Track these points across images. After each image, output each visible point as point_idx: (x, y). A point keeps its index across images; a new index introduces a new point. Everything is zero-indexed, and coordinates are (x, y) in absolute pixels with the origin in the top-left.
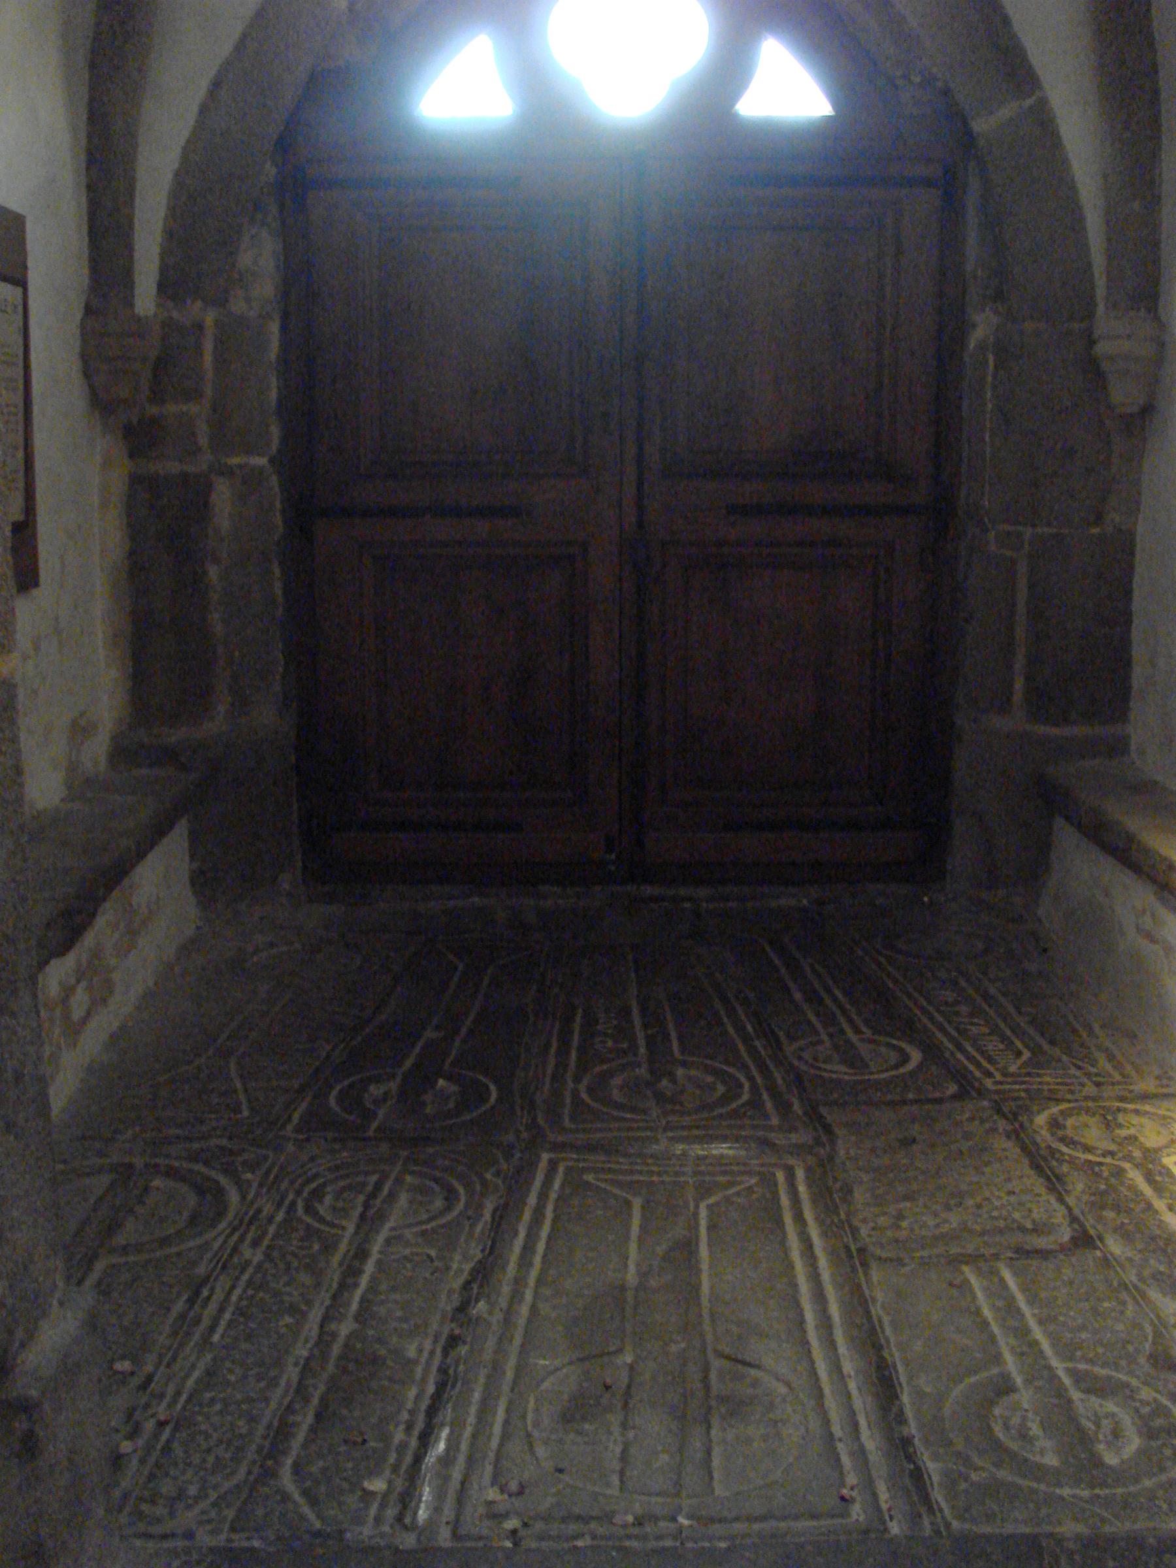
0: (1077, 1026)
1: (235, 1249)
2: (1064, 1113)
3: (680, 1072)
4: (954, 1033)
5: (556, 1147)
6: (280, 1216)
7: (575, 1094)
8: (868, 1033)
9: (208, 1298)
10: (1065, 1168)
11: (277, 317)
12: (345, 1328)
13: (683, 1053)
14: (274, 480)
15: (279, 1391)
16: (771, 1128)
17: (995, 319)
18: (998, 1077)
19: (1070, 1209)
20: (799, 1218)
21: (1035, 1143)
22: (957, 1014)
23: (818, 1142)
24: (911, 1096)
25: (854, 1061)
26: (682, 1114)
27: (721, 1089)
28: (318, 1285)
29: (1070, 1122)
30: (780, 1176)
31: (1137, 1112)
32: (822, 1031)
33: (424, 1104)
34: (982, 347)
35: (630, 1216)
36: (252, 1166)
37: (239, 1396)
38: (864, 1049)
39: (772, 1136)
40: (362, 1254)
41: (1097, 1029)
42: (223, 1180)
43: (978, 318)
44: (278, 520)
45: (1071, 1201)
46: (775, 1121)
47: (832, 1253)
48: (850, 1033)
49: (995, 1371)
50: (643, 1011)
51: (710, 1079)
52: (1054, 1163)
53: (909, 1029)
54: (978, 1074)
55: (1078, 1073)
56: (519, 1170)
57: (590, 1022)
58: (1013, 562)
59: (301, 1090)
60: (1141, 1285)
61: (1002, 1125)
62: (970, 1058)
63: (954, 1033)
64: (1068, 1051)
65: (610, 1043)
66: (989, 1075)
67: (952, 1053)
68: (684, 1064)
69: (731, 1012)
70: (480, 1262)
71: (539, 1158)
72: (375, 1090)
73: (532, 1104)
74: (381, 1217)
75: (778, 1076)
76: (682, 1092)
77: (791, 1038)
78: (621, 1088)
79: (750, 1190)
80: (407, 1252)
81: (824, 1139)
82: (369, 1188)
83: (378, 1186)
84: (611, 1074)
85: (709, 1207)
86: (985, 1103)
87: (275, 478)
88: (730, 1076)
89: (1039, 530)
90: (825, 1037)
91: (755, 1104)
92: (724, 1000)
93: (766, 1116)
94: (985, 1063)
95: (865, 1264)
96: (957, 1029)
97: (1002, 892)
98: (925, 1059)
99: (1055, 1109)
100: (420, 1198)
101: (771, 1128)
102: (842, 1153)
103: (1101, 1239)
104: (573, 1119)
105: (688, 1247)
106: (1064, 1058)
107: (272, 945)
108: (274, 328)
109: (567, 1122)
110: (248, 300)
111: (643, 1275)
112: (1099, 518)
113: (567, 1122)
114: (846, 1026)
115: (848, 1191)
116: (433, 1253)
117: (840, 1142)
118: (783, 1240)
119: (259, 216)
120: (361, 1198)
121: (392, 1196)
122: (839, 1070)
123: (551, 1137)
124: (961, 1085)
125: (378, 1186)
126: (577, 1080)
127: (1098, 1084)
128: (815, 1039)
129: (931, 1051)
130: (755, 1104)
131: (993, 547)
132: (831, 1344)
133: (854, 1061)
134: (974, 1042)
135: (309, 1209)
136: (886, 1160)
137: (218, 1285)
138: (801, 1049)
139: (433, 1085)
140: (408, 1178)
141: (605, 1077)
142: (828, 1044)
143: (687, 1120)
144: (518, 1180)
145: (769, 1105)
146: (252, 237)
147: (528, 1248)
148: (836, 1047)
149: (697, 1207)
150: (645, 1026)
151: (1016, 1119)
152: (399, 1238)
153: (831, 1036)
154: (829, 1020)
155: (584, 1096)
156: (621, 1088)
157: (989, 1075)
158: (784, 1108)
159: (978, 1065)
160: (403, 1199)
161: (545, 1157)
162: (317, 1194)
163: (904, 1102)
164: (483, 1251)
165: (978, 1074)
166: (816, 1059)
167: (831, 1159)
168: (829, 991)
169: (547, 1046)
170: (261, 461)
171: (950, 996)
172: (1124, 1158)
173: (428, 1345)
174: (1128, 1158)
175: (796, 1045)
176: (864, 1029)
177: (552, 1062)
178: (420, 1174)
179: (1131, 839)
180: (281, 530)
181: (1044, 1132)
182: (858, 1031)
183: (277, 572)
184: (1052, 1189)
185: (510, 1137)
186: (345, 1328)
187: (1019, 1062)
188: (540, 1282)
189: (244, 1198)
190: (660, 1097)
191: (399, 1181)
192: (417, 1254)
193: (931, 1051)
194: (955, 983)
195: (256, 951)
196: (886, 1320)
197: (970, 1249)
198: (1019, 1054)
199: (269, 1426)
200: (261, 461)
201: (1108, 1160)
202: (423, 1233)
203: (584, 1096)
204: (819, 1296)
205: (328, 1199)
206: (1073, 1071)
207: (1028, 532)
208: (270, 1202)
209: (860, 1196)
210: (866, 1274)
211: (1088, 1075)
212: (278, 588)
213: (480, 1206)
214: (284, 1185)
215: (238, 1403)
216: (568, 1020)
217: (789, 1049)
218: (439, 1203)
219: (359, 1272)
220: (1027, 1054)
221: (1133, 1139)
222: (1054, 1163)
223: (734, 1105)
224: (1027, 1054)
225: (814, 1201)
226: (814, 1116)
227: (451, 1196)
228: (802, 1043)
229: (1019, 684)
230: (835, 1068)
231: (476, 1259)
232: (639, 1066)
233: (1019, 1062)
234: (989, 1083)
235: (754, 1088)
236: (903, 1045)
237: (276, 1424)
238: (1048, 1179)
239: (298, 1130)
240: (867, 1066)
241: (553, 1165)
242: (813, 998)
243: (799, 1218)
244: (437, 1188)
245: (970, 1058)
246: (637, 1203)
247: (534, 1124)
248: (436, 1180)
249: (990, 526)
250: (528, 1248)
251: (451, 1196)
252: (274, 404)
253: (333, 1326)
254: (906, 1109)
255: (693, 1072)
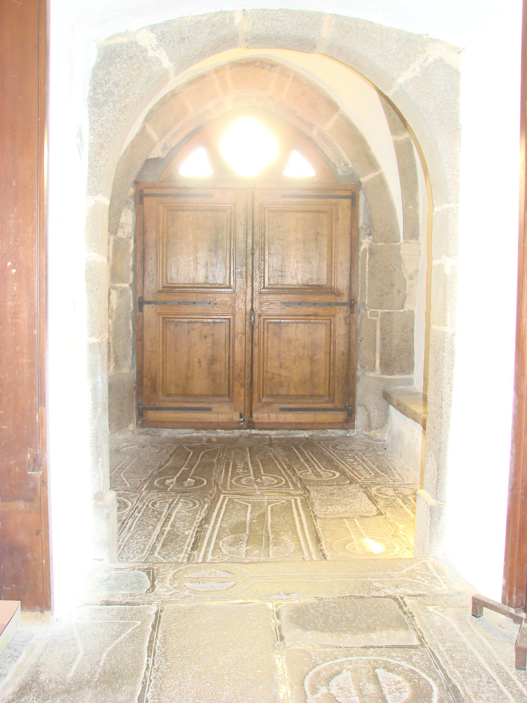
0: (391, 468)
1: (132, 514)
2: (381, 488)
3: (263, 477)
4: (351, 469)
5: (224, 494)
6: (145, 507)
7: (231, 482)
8: (324, 469)
9: (127, 523)
10: (378, 499)
11: (133, 238)
13: (264, 473)
14: (131, 292)
15: (151, 540)
16: (291, 490)
17: (369, 241)
18: (363, 479)
19: (377, 508)
20: (297, 509)
21: (371, 494)
22: (353, 465)
23: (305, 493)
24: (335, 484)
25: (317, 474)
26: (264, 487)
27: (276, 481)
28: (158, 521)
29: (383, 489)
30: (293, 501)
31: (404, 487)
32: (309, 468)
34: (365, 250)
36: (133, 497)
37: (140, 541)
38: (322, 473)
39: (291, 492)
40: (170, 515)
41: (397, 469)
42: (126, 500)
43: (363, 241)
44: (132, 305)
45: (378, 506)
46: (292, 488)
47: (307, 516)
48: (318, 469)
49: (349, 538)
50: (252, 463)
51: (273, 479)
52: (376, 498)
53: (337, 468)
54: (357, 478)
55: (389, 479)
56: (214, 498)
57: (235, 466)
58: (375, 321)
59: (145, 481)
60: (394, 522)
61: (362, 490)
62: (355, 475)
63: (351, 469)
64: (386, 473)
65: (241, 471)
66: (360, 478)
67: (350, 474)
68: (264, 476)
69: (280, 464)
71: (220, 496)
72: (168, 481)
73: (218, 485)
74: (174, 508)
75: (294, 478)
76: (264, 482)
77: (299, 470)
78: (245, 481)
79: (283, 503)
81: (307, 493)
82: (170, 502)
84: (242, 478)
85: (271, 507)
86: (358, 485)
87: (131, 291)
88: (279, 478)
89: (383, 311)
90: (309, 469)
91: (287, 484)
92: (278, 461)
93: (289, 487)
94: (359, 476)
95: (315, 519)
96: (352, 468)
97: (373, 432)
98: (340, 475)
99: (379, 487)
101: (291, 490)
102: (312, 496)
103: (385, 514)
104: (230, 488)
105: (264, 515)
106: (385, 475)
107: (128, 446)
108: (132, 241)
109: (228, 488)
110: (124, 233)
111: (252, 520)
112: (402, 307)
113: (228, 488)
114: (316, 467)
115: (313, 504)
117: (311, 493)
118: (292, 514)
119: (128, 205)
120: (168, 504)
121: (177, 504)
122: (313, 477)
123: (223, 491)
124: (350, 481)
126: (231, 479)
127: (394, 481)
128: (306, 470)
129: (343, 473)
130: (287, 484)
131: (369, 316)
132: (304, 533)
133: (317, 474)
134: (357, 471)
135: (153, 505)
136: (325, 498)
137: (130, 521)
138: (302, 473)
139: (187, 480)
141: (240, 479)
142: (311, 471)
143: (265, 488)
144: (214, 502)
145: (291, 485)
146: (126, 212)
147: (218, 516)
148: (313, 472)
149: (267, 506)
150: (253, 467)
151: (366, 488)
152: (181, 512)
153: (312, 470)
154: (311, 466)
155: (234, 483)
156: (245, 481)
157: (360, 478)
158: (295, 485)
159: (357, 476)
160: (180, 504)
161: (222, 496)
162: (155, 503)
163: (332, 485)
165: (357, 478)
166: (306, 475)
167: (308, 497)
168: (312, 459)
169: (222, 471)
170: (127, 285)
171: (352, 460)
172: (397, 497)
173: (191, 532)
174: (399, 497)
175: (301, 472)
176: (322, 468)
177: (223, 475)
178: (185, 499)
179: (406, 407)
180: (132, 308)
181: (374, 492)
182: (320, 468)
183: (131, 322)
184: (374, 503)
185: (211, 492)
186: (168, 529)
187: (370, 476)
188: (222, 520)
189: (132, 504)
190: (257, 483)
191: (179, 500)
193: (343, 473)
194: (354, 457)
195: (123, 448)
196: (320, 529)
197: (347, 516)
198: (371, 474)
199: (150, 546)
200: (127, 285)
201: (392, 497)
202: (187, 511)
203: (234, 483)
204: (301, 524)
205: (158, 504)
206: (387, 478)
207: (380, 311)
209: (316, 505)
210: (315, 521)
211: (391, 479)
212: (131, 327)
214: (145, 501)
215: (141, 542)
216: (228, 465)
217: (298, 473)
218: (191, 505)
219: (170, 518)
220: (373, 474)
221: (401, 493)
222: (376, 498)
223: (280, 485)
224: (373, 474)
225: (302, 506)
226: (304, 488)
227: (195, 504)
228: (302, 471)
229: (378, 361)
230: (312, 477)
232: (251, 476)
233: (370, 476)
234: (360, 481)
235: (286, 481)
236: (334, 472)
237: (152, 546)
238: (373, 501)
239: (146, 489)
240: (322, 477)
241: (224, 498)
242: (307, 460)
243: (297, 509)
244: (190, 502)
245: (355, 475)
246: (250, 505)
247: (218, 488)
249: (368, 309)
250: (218, 516)
251: (195, 504)
252: (131, 266)
253: (164, 528)
254: (333, 487)
255: (267, 477)
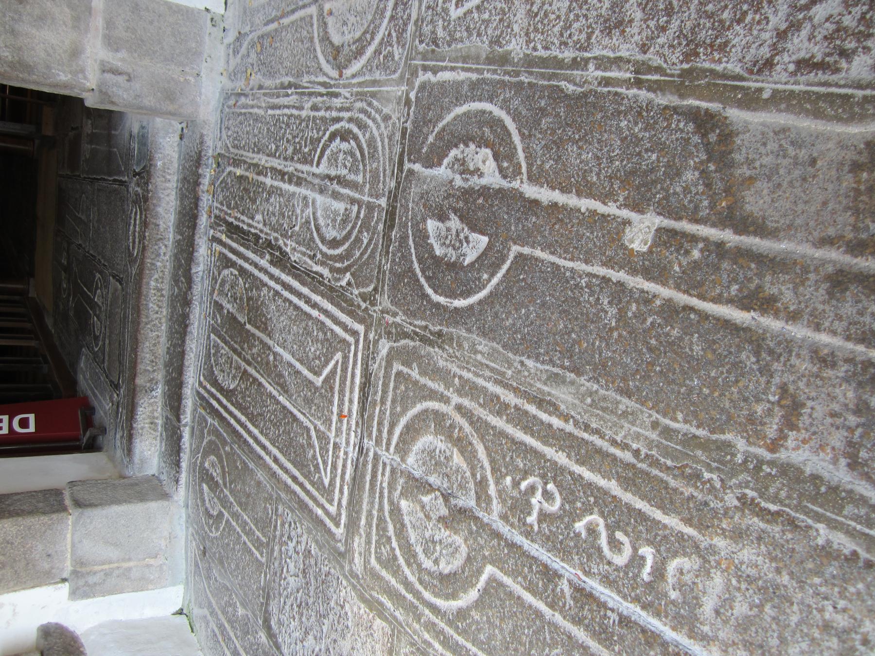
12: (268, 181)
28: (285, 159)
33: (442, 218)
35: (448, 124)
56: (350, 303)
70: (289, 258)
80: (299, 211)
83: (354, 186)
100: (339, 219)
116: (297, 228)
125: (354, 186)
140: (355, 208)
160: (340, 206)
164: (295, 261)
192: (296, 218)
202: (308, 222)
205: (345, 146)
208: (440, 357)
213: (323, 264)
231: (291, 256)
248: (349, 233)
